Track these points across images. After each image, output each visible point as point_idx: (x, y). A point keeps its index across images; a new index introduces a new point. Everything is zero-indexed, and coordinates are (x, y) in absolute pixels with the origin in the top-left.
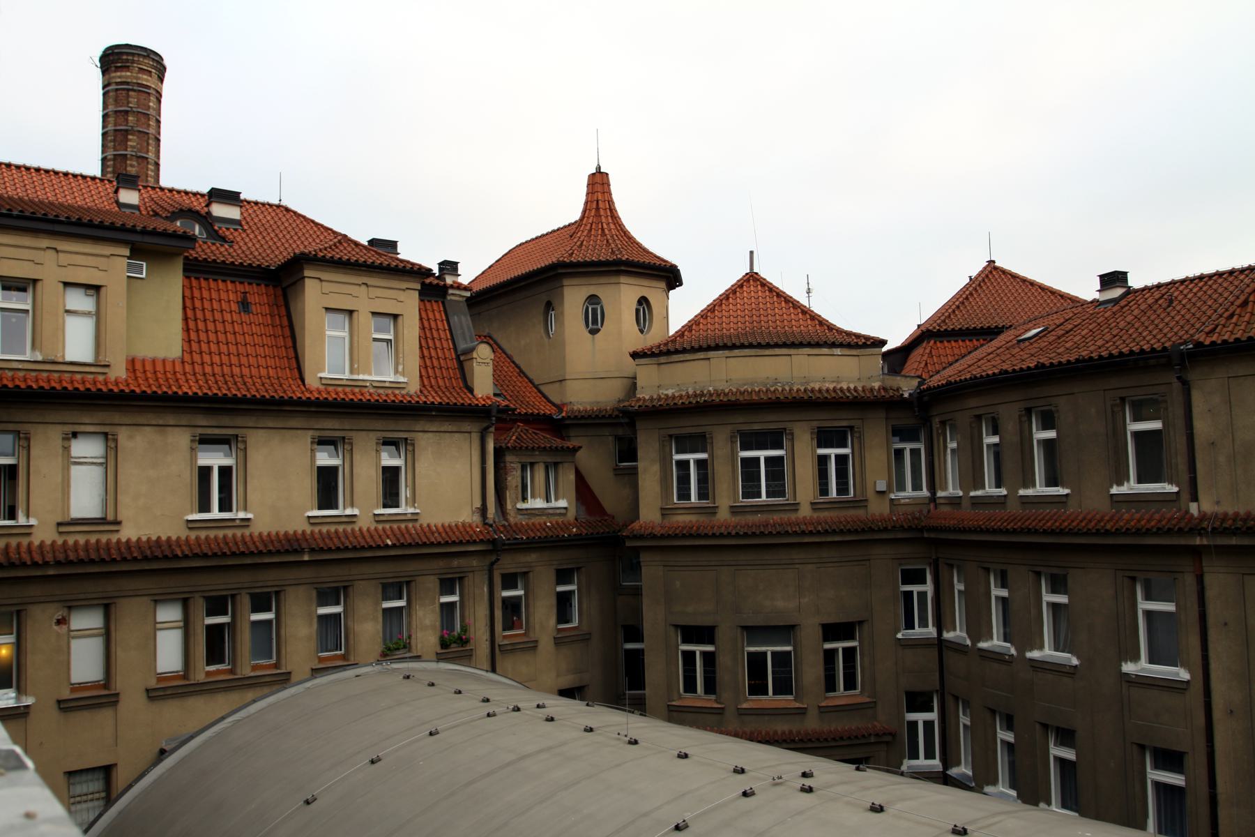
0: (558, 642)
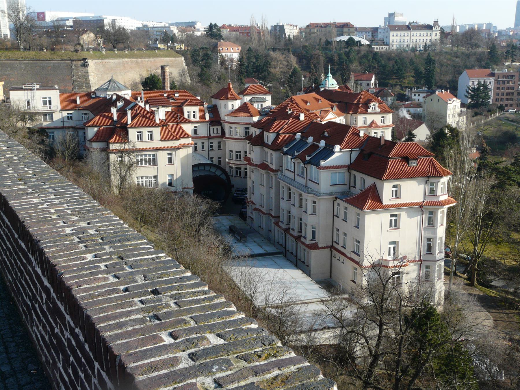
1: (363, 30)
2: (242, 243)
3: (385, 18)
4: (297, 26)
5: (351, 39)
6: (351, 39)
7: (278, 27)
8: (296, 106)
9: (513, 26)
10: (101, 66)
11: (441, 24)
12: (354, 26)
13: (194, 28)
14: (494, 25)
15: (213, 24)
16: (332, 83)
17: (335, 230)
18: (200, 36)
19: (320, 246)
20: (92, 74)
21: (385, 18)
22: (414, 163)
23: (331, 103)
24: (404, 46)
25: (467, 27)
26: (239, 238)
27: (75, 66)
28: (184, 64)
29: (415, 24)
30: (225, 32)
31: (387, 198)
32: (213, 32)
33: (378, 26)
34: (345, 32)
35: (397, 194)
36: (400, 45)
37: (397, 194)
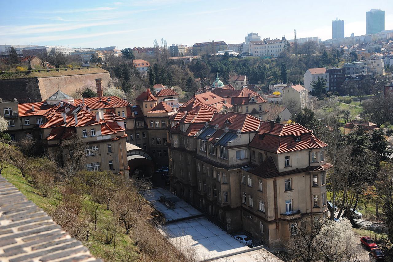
0: (143, 139)
1: (233, 46)
2: (172, 209)
3: (246, 37)
4: (186, 46)
5: (226, 54)
6: (226, 54)
7: (173, 47)
8: (198, 101)
9: (332, 39)
10: (48, 82)
11: (287, 39)
12: (227, 44)
13: (114, 51)
14: (319, 38)
15: (127, 48)
16: (219, 83)
17: (313, 196)
18: (119, 57)
19: (232, 207)
20: (42, 88)
21: (246, 37)
22: (299, 139)
23: (222, 98)
24: (263, 55)
25: (308, 40)
26: (169, 206)
27: (28, 83)
28: (110, 77)
29: (269, 40)
30: (135, 54)
31: (281, 166)
32: (127, 53)
33: (243, 43)
34: (221, 48)
35: (288, 164)
36: (260, 55)
37: (288, 164)
